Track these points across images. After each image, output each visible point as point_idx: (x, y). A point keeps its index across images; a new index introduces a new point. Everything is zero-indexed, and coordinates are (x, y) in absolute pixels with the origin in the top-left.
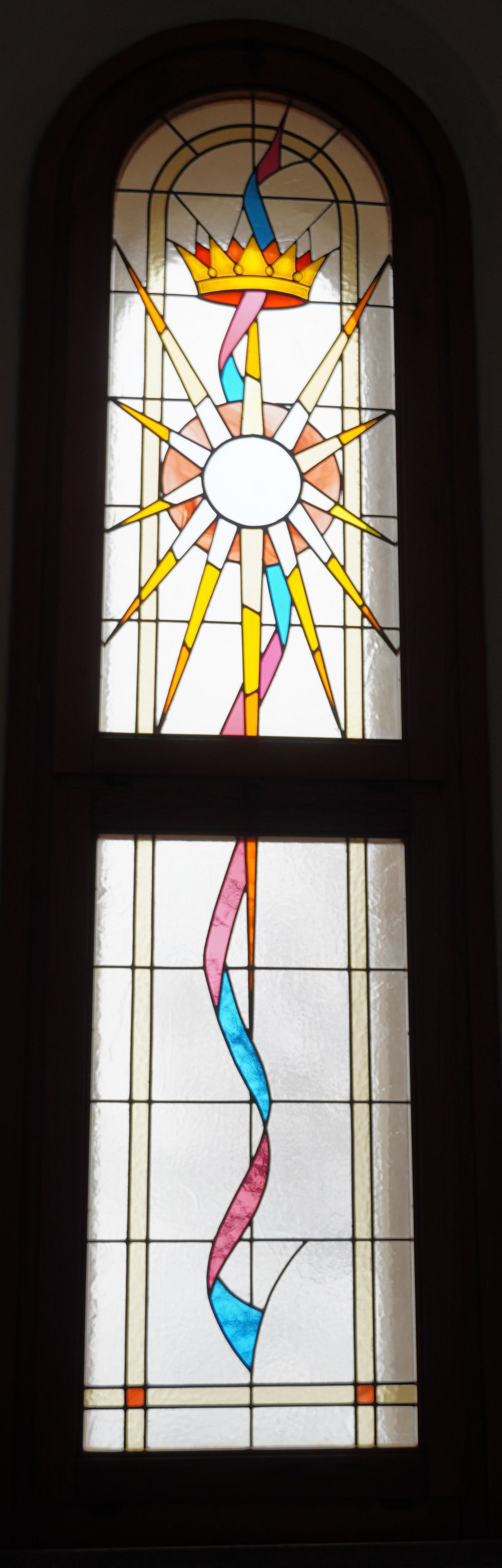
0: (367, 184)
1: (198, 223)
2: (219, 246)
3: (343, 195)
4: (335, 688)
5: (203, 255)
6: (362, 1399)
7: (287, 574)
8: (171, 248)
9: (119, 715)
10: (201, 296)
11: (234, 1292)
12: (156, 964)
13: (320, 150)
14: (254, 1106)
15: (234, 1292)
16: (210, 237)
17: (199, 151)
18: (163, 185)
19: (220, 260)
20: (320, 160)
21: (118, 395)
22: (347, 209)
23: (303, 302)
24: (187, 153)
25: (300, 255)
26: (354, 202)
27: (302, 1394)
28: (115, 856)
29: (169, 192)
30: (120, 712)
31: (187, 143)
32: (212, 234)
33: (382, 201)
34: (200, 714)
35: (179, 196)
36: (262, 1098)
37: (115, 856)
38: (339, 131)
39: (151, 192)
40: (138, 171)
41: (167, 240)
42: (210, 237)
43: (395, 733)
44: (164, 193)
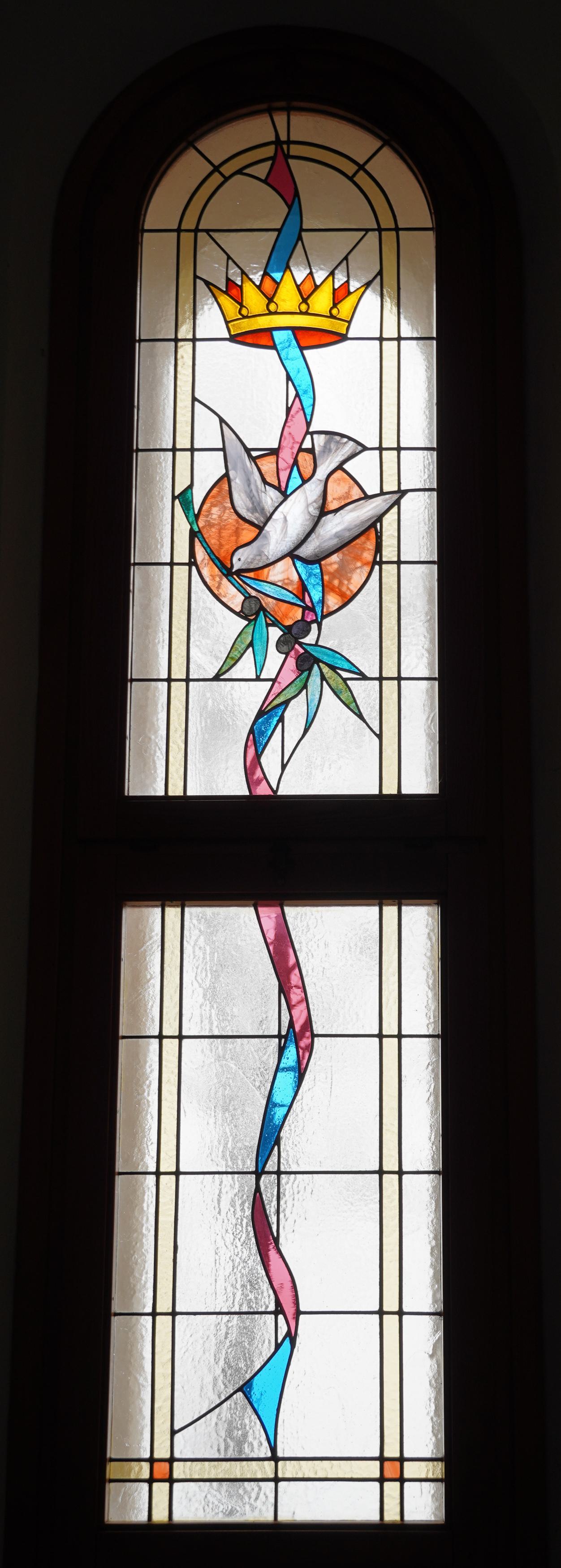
0: (412, 203)
1: (229, 258)
2: (251, 280)
3: (387, 221)
4: (193, 964)
5: (233, 290)
6: (387, 1474)
7: (177, 1427)
8: (200, 284)
9: (420, 923)
10: (234, 338)
11: (298, 392)
12: (185, 1041)
13: (361, 167)
14: (281, 1317)
15: (298, 392)
16: (243, 273)
17: (227, 175)
18: (189, 223)
19: (253, 299)
20: (361, 178)
21: (216, 671)
22: (389, 237)
23: (342, 338)
24: (217, 179)
25: (337, 286)
26: (397, 229)
27: (327, 1468)
28: (420, 777)
29: (196, 231)
30: (420, 925)
31: (216, 169)
32: (246, 270)
33: (431, 226)
34: (218, 775)
35: (211, 233)
36: (289, 1310)
37: (420, 777)
38: (386, 143)
39: (179, 230)
40: (163, 207)
41: (196, 277)
42: (243, 273)
43: (438, 792)
44: (191, 232)
